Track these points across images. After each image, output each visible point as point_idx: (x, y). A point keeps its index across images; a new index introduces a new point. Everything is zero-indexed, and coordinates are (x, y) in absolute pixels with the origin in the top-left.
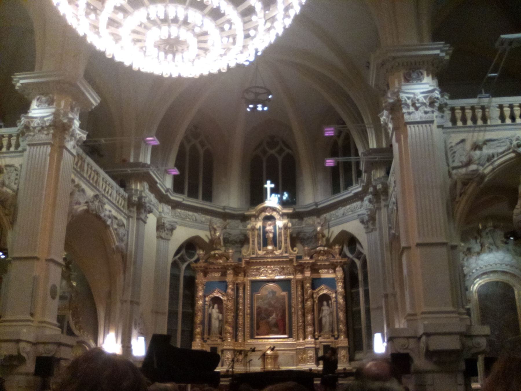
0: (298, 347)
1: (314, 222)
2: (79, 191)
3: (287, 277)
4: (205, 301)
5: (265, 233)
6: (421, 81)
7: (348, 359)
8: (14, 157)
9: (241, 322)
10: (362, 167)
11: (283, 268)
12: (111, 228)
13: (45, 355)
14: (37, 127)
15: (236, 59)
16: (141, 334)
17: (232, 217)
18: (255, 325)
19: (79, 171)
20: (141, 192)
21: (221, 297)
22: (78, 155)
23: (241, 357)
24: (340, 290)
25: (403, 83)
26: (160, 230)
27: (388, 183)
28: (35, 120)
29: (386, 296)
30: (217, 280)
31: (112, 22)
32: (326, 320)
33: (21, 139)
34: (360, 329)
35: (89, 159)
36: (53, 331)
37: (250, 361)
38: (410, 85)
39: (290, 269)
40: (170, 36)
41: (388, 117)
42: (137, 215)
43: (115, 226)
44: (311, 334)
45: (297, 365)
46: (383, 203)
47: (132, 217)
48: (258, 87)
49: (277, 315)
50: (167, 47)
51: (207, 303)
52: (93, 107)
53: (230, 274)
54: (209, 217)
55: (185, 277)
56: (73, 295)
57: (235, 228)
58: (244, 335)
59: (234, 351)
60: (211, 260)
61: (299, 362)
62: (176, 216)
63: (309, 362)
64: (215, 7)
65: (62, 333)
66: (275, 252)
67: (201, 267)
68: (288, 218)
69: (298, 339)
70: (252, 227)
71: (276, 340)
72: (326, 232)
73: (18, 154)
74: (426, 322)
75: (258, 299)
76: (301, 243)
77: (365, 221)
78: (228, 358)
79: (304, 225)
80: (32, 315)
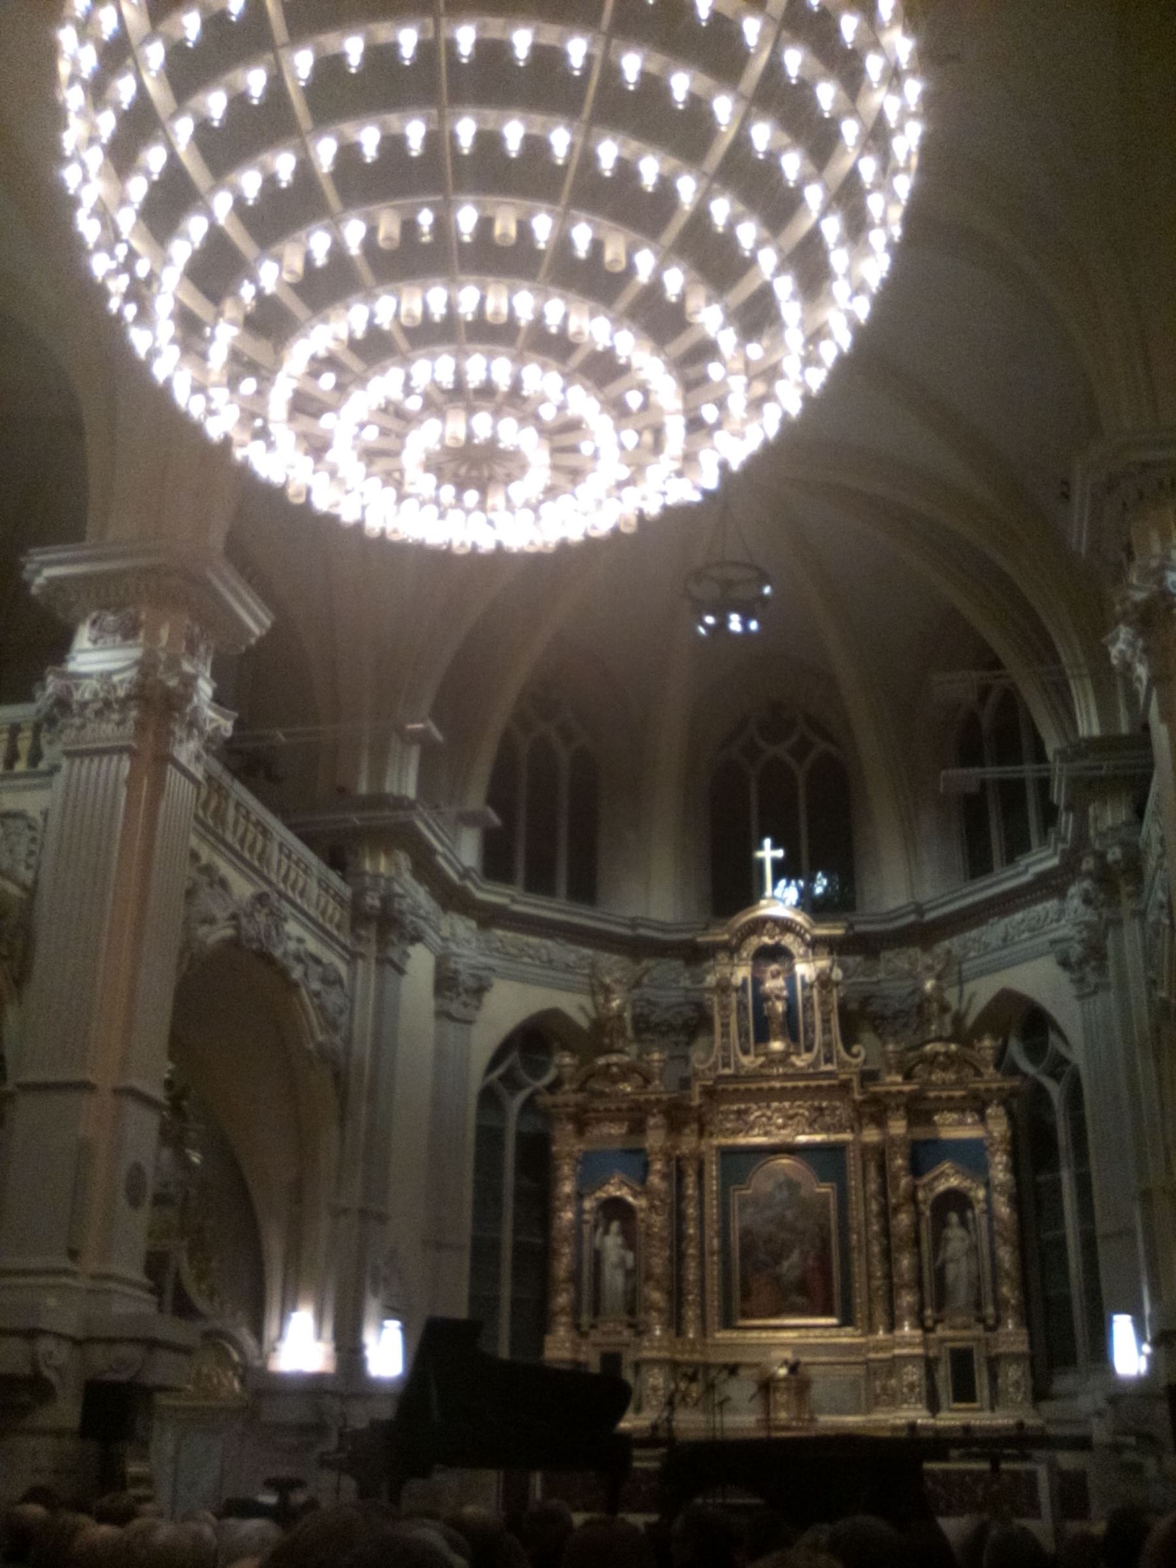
0: (872, 1355)
2: (211, 885)
3: (833, 1137)
4: (580, 1212)
5: (761, 999)
7: (1030, 1396)
8: (25, 788)
9: (691, 1274)
10: (1059, 794)
11: (821, 1110)
12: (304, 992)
13: (110, 1377)
14: (93, 701)
16: (392, 1311)
17: (661, 950)
19: (211, 825)
20: (390, 880)
21: (630, 1199)
22: (210, 778)
23: (695, 1390)
27: (1141, 845)
28: (87, 682)
29: (1146, 1196)
30: (618, 1146)
31: (304, 406)
32: (959, 1271)
33: (44, 738)
34: (1067, 1301)
35: (239, 791)
36: (132, 1305)
37: (721, 1404)
39: (843, 1111)
40: (470, 436)
41: (1131, 645)
42: (379, 950)
43: (316, 986)
45: (869, 1411)
46: (1128, 905)
47: (362, 956)
48: (735, 564)
50: (463, 471)
51: (587, 1217)
52: (253, 641)
53: (656, 1127)
54: (587, 952)
55: (520, 1136)
56: (193, 1192)
57: (669, 984)
58: (703, 1317)
59: (674, 1365)
60: (597, 1085)
61: (875, 1402)
62: (491, 950)
63: (905, 1401)
64: (600, 348)
65: (160, 1305)
66: (794, 1059)
67: (566, 1105)
68: (831, 953)
69: (871, 1329)
71: (803, 1332)
72: (951, 996)
73: (37, 781)
75: (744, 1205)
77: (1073, 960)
78: (655, 1389)
79: (881, 975)
80: (73, 1254)
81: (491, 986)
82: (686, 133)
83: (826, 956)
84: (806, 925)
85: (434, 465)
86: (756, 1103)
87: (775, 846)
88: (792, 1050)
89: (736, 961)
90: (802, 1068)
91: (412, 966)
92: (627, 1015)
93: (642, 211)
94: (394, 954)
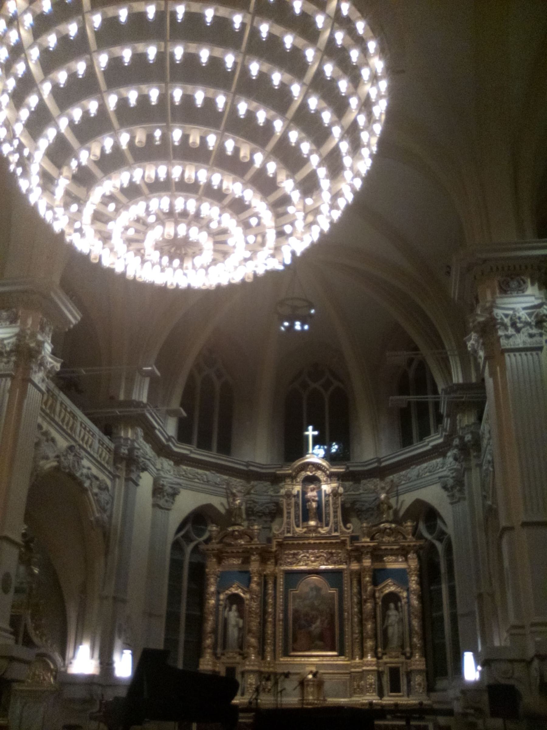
0: (353, 670)
1: (376, 486)
2: (47, 441)
4: (218, 600)
5: (306, 501)
6: (523, 292)
10: (443, 409)
11: (331, 553)
12: (90, 493)
15: (266, 265)
16: (127, 646)
17: (260, 477)
18: (290, 636)
20: (133, 441)
21: (242, 594)
22: (48, 390)
24: (414, 586)
25: (498, 295)
26: (158, 495)
29: (480, 596)
30: (236, 569)
31: (99, 217)
32: (394, 631)
34: (444, 645)
35: (62, 397)
37: (281, 692)
38: (507, 297)
39: (342, 555)
40: (176, 234)
41: (477, 341)
42: (127, 475)
43: (96, 490)
44: (371, 650)
45: (351, 696)
46: (474, 462)
47: (119, 477)
49: (322, 622)
50: (173, 250)
51: (221, 602)
52: (72, 326)
55: (191, 563)
57: (263, 493)
58: (274, 651)
59: (260, 673)
60: (228, 540)
62: (180, 475)
63: (368, 692)
64: (237, 196)
65: (17, 642)
66: (320, 529)
67: (213, 550)
68: (338, 480)
69: (353, 658)
70: (286, 492)
71: (321, 658)
72: (393, 501)
74: (538, 639)
75: (294, 597)
76: (358, 516)
78: (251, 684)
79: (361, 491)
81: (179, 492)
82: (279, 100)
83: (336, 481)
84: (328, 467)
85: (158, 247)
86: (302, 550)
87: (314, 430)
88: (319, 525)
89: (294, 483)
90: (324, 534)
91: (141, 482)
92: (243, 507)
93: (259, 135)
94: (134, 476)
